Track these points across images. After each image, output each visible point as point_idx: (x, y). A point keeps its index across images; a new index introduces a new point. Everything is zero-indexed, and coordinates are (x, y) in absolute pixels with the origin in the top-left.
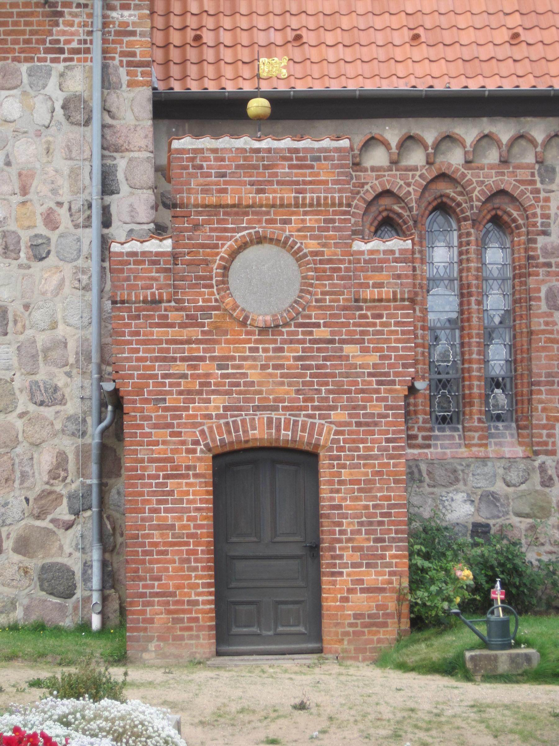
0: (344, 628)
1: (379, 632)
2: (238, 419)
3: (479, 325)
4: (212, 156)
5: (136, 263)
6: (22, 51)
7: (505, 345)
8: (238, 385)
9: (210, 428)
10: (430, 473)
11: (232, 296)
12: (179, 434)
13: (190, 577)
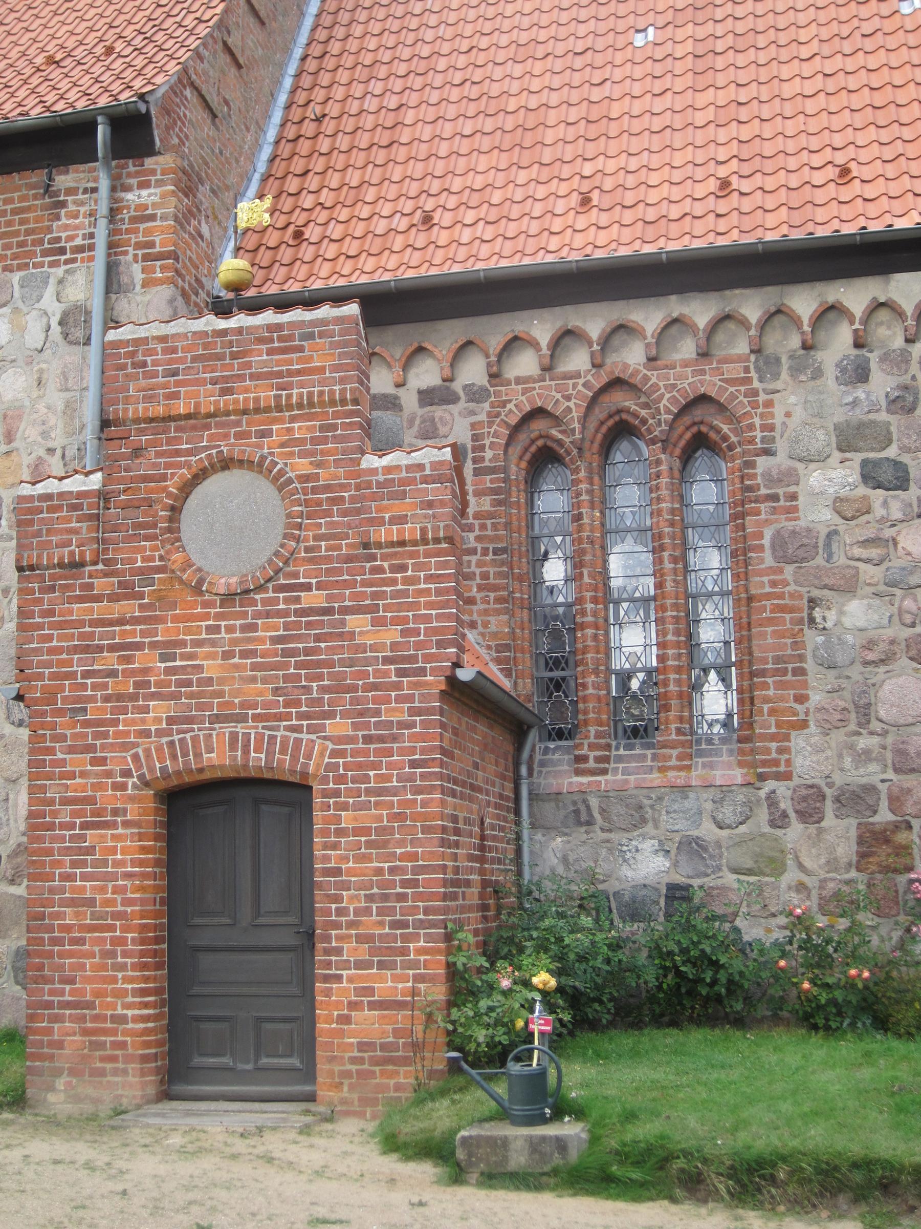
0: (344, 1064)
1: (397, 1073)
2: (188, 736)
3: (677, 592)
4: (159, 347)
5: (51, 509)
6: (15, 257)
7: (723, 620)
8: (189, 683)
9: (147, 751)
10: (604, 810)
11: (184, 551)
12: (103, 761)
13: (114, 980)
